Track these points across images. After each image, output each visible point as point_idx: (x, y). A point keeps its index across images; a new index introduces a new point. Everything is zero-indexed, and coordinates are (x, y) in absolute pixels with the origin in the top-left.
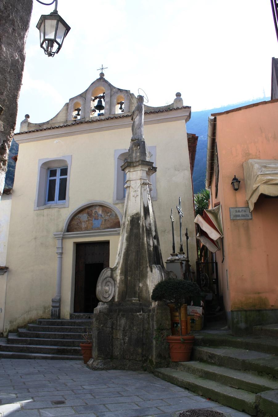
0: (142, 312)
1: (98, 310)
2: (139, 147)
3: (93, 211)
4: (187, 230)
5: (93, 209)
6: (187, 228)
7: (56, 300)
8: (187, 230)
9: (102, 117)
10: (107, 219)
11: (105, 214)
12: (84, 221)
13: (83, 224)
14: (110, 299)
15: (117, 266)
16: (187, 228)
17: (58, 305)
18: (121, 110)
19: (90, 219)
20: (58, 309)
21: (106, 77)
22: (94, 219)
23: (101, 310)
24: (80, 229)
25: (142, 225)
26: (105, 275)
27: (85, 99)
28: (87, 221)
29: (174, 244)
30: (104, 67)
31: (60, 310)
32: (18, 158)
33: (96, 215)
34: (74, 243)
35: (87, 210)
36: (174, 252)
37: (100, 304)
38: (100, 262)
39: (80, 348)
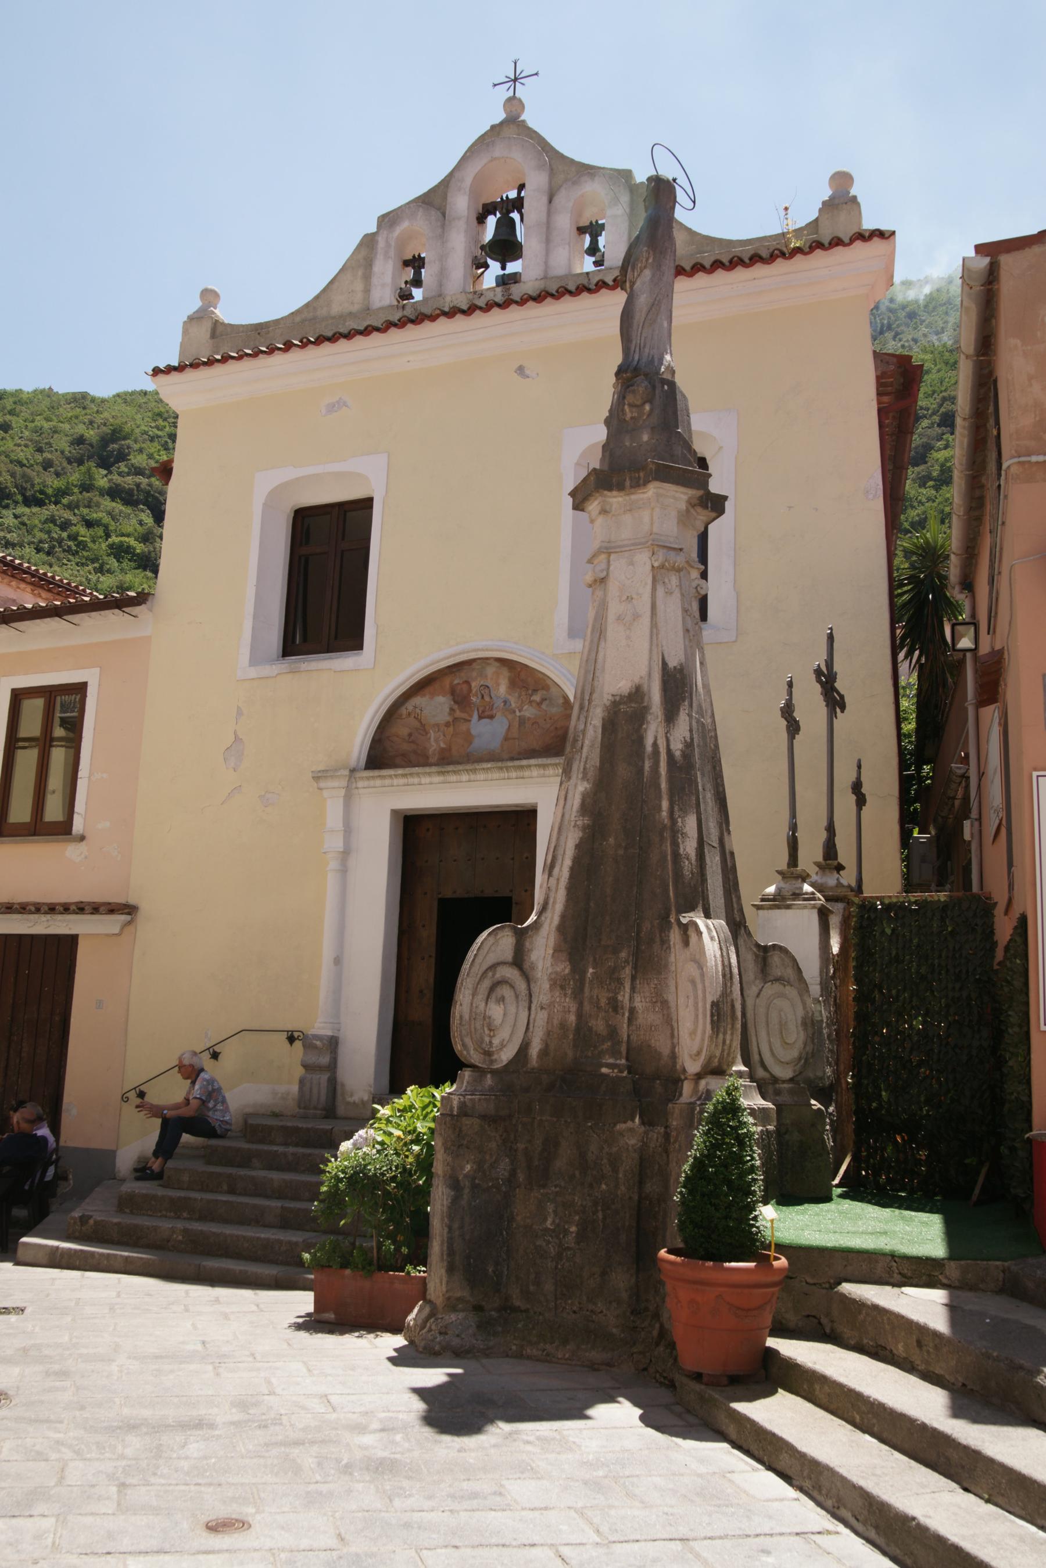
0: (637, 1120)
2: (647, 407)
3: (473, 684)
4: (859, 767)
5: (474, 674)
6: (859, 761)
8: (859, 767)
9: (517, 291)
10: (529, 718)
11: (520, 696)
12: (438, 725)
13: (432, 734)
14: (506, 1056)
16: (859, 761)
17: (325, 1060)
18: (593, 259)
19: (458, 714)
20: (324, 1077)
21: (530, 117)
22: (475, 716)
23: (469, 1104)
25: (655, 745)
26: (491, 955)
27: (444, 216)
28: (447, 724)
29: (794, 828)
33: (487, 699)
34: (395, 813)
35: (447, 682)
36: (793, 859)
38: (482, 892)
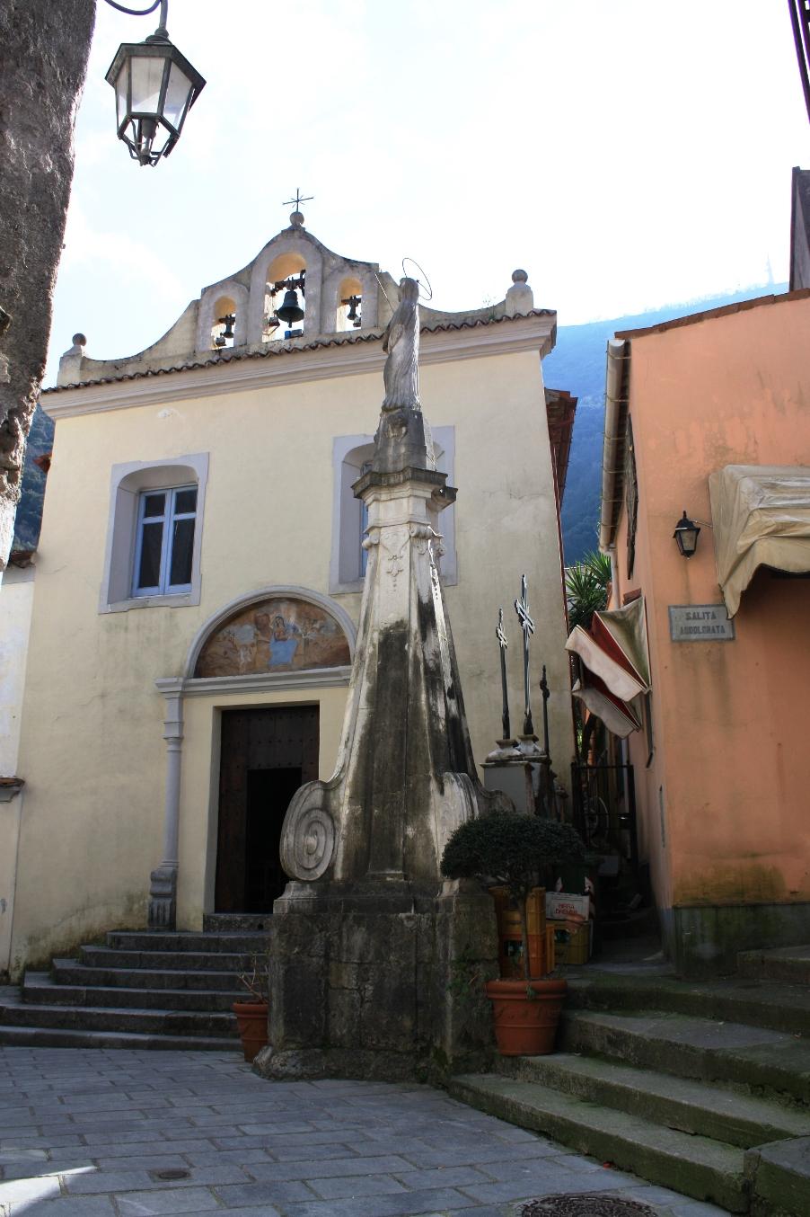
0: (413, 911)
1: (286, 904)
3: (271, 616)
4: (544, 670)
5: (272, 609)
6: (544, 667)
7: (163, 877)
8: (544, 670)
9: (298, 342)
10: (311, 640)
11: (305, 624)
13: (242, 653)
14: (320, 871)
15: (342, 776)
16: (544, 667)
17: (168, 889)
18: (352, 322)
19: (261, 638)
20: (168, 901)
21: (308, 226)
22: (273, 640)
23: (296, 906)
24: (233, 668)
25: (415, 656)
26: (307, 803)
27: (249, 290)
28: (253, 645)
29: (506, 711)
30: (303, 194)
31: (173, 905)
32: (52, 462)
33: (281, 626)
34: (216, 708)
35: (252, 614)
36: (507, 735)
37: (293, 888)
38: (290, 764)
39: (233, 1017)
